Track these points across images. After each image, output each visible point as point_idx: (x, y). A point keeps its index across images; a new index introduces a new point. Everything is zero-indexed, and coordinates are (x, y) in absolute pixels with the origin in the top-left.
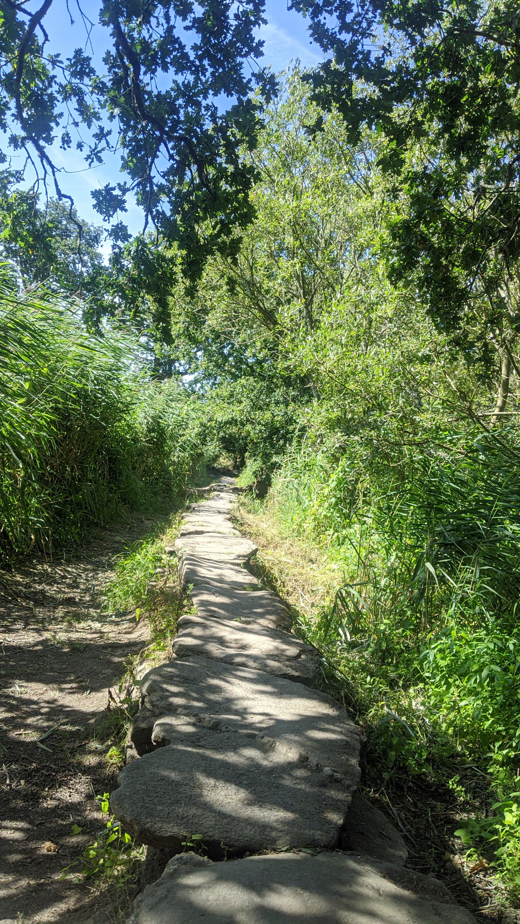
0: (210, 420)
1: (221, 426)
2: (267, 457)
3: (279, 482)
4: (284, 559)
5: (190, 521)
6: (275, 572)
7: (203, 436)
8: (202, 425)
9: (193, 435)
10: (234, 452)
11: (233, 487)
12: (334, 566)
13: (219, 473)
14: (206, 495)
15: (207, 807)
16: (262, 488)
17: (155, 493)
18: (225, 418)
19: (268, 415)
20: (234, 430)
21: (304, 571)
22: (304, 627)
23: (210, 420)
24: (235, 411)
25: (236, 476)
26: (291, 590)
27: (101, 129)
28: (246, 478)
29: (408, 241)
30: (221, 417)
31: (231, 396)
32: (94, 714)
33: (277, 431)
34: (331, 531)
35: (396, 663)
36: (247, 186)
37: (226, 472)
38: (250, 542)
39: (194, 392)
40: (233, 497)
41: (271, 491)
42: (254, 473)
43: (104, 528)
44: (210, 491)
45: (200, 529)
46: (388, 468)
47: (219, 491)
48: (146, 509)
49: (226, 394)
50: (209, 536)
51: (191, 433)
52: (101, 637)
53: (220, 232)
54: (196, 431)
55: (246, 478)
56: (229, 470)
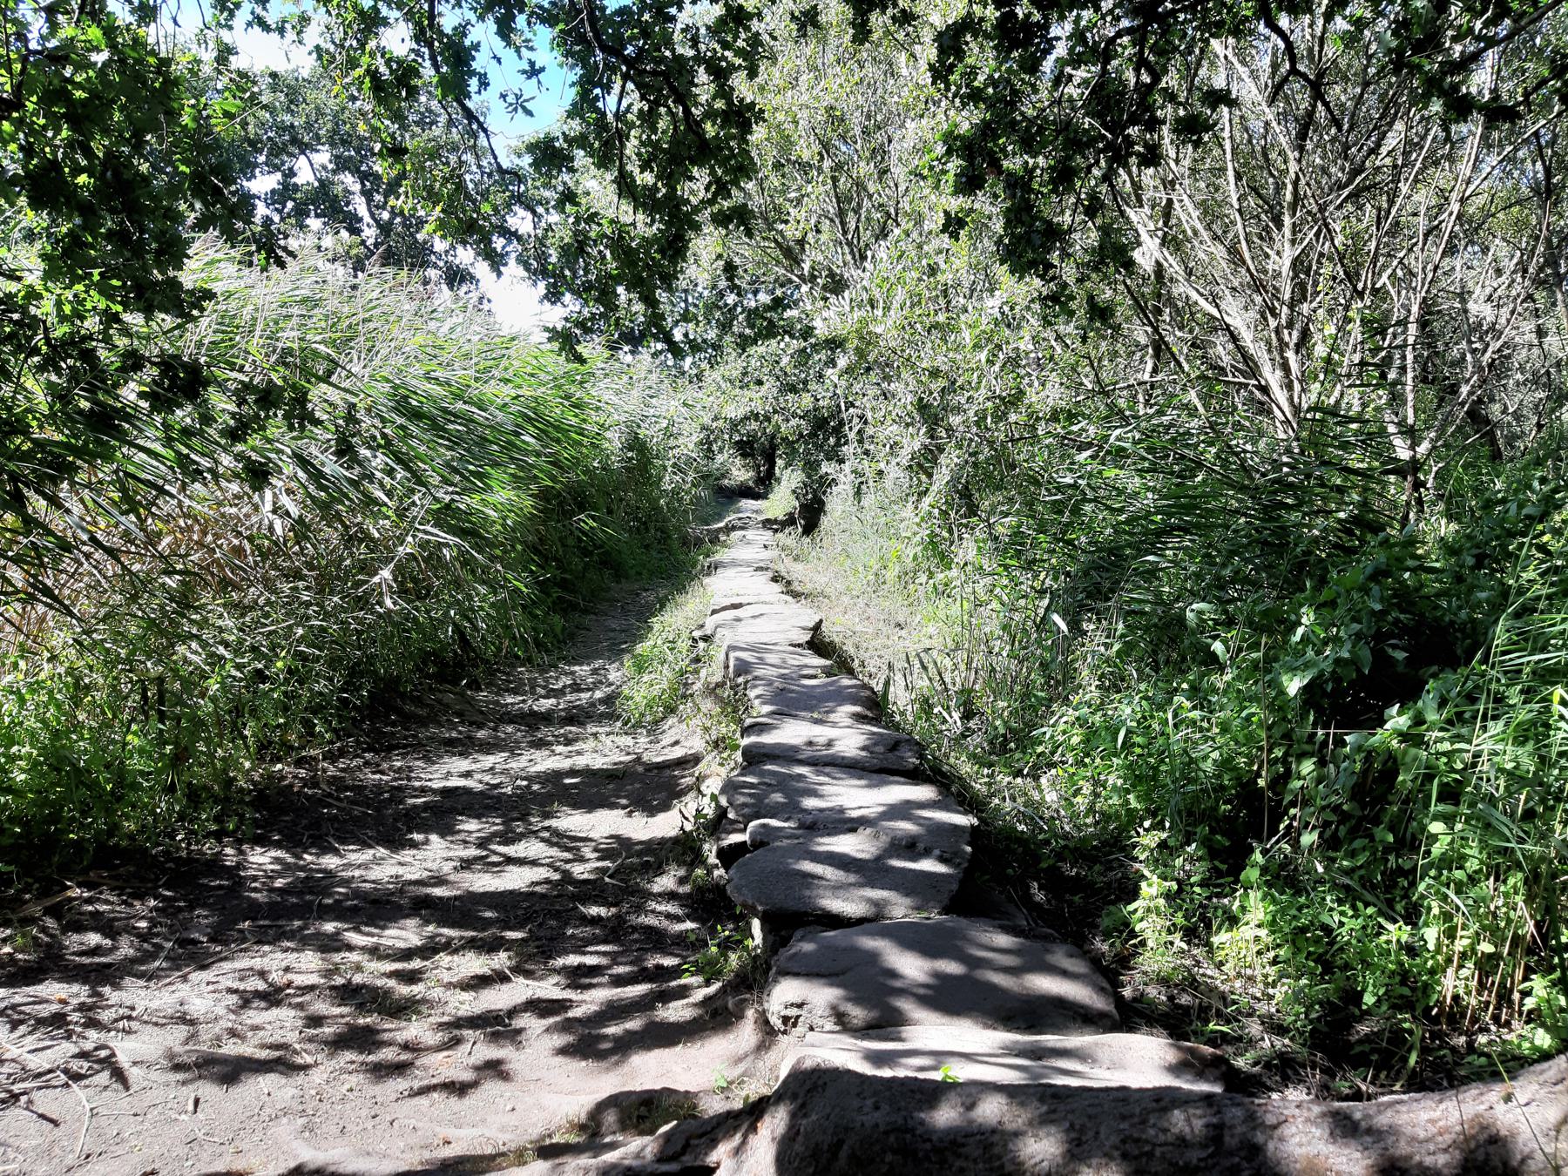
0: (716, 419)
1: (734, 425)
2: (811, 467)
3: (837, 503)
4: (858, 628)
5: (718, 587)
6: (850, 649)
7: (707, 447)
8: (703, 428)
9: (691, 446)
10: (753, 456)
11: (761, 518)
12: (931, 630)
13: (732, 495)
14: (723, 538)
15: (805, 811)
16: (810, 515)
17: (647, 547)
18: (740, 413)
19: (806, 401)
20: (754, 425)
21: (890, 643)
22: (898, 718)
23: (716, 419)
24: (757, 399)
25: (764, 496)
26: (873, 670)
27: (532, 64)
28: (781, 501)
29: (975, 159)
30: (734, 411)
31: (745, 374)
32: (641, 843)
33: (825, 421)
34: (923, 578)
35: (1013, 745)
36: (746, 128)
37: (746, 492)
38: (810, 611)
39: (683, 373)
40: (767, 536)
41: (825, 522)
42: (794, 492)
43: (586, 611)
44: (729, 529)
45: (736, 600)
46: (986, 482)
47: (742, 528)
48: (640, 574)
49: (736, 373)
50: (743, 601)
51: (688, 444)
52: (192, 1037)
53: (715, 195)
54: (695, 438)
55: (781, 501)
56: (750, 488)
